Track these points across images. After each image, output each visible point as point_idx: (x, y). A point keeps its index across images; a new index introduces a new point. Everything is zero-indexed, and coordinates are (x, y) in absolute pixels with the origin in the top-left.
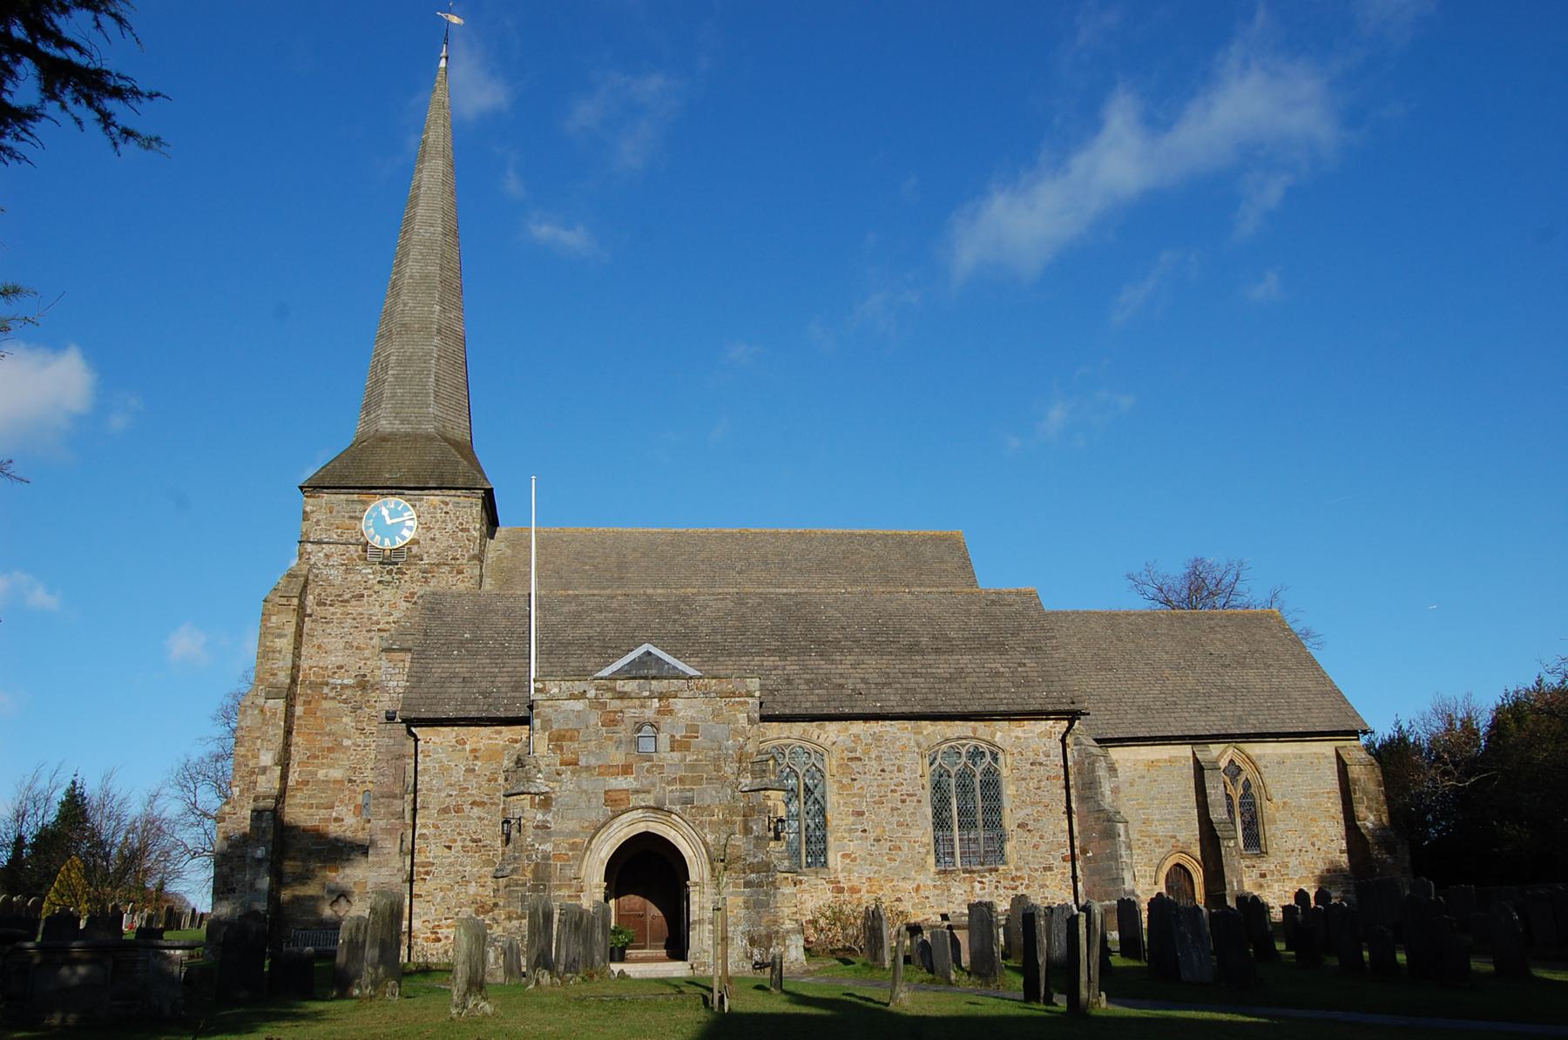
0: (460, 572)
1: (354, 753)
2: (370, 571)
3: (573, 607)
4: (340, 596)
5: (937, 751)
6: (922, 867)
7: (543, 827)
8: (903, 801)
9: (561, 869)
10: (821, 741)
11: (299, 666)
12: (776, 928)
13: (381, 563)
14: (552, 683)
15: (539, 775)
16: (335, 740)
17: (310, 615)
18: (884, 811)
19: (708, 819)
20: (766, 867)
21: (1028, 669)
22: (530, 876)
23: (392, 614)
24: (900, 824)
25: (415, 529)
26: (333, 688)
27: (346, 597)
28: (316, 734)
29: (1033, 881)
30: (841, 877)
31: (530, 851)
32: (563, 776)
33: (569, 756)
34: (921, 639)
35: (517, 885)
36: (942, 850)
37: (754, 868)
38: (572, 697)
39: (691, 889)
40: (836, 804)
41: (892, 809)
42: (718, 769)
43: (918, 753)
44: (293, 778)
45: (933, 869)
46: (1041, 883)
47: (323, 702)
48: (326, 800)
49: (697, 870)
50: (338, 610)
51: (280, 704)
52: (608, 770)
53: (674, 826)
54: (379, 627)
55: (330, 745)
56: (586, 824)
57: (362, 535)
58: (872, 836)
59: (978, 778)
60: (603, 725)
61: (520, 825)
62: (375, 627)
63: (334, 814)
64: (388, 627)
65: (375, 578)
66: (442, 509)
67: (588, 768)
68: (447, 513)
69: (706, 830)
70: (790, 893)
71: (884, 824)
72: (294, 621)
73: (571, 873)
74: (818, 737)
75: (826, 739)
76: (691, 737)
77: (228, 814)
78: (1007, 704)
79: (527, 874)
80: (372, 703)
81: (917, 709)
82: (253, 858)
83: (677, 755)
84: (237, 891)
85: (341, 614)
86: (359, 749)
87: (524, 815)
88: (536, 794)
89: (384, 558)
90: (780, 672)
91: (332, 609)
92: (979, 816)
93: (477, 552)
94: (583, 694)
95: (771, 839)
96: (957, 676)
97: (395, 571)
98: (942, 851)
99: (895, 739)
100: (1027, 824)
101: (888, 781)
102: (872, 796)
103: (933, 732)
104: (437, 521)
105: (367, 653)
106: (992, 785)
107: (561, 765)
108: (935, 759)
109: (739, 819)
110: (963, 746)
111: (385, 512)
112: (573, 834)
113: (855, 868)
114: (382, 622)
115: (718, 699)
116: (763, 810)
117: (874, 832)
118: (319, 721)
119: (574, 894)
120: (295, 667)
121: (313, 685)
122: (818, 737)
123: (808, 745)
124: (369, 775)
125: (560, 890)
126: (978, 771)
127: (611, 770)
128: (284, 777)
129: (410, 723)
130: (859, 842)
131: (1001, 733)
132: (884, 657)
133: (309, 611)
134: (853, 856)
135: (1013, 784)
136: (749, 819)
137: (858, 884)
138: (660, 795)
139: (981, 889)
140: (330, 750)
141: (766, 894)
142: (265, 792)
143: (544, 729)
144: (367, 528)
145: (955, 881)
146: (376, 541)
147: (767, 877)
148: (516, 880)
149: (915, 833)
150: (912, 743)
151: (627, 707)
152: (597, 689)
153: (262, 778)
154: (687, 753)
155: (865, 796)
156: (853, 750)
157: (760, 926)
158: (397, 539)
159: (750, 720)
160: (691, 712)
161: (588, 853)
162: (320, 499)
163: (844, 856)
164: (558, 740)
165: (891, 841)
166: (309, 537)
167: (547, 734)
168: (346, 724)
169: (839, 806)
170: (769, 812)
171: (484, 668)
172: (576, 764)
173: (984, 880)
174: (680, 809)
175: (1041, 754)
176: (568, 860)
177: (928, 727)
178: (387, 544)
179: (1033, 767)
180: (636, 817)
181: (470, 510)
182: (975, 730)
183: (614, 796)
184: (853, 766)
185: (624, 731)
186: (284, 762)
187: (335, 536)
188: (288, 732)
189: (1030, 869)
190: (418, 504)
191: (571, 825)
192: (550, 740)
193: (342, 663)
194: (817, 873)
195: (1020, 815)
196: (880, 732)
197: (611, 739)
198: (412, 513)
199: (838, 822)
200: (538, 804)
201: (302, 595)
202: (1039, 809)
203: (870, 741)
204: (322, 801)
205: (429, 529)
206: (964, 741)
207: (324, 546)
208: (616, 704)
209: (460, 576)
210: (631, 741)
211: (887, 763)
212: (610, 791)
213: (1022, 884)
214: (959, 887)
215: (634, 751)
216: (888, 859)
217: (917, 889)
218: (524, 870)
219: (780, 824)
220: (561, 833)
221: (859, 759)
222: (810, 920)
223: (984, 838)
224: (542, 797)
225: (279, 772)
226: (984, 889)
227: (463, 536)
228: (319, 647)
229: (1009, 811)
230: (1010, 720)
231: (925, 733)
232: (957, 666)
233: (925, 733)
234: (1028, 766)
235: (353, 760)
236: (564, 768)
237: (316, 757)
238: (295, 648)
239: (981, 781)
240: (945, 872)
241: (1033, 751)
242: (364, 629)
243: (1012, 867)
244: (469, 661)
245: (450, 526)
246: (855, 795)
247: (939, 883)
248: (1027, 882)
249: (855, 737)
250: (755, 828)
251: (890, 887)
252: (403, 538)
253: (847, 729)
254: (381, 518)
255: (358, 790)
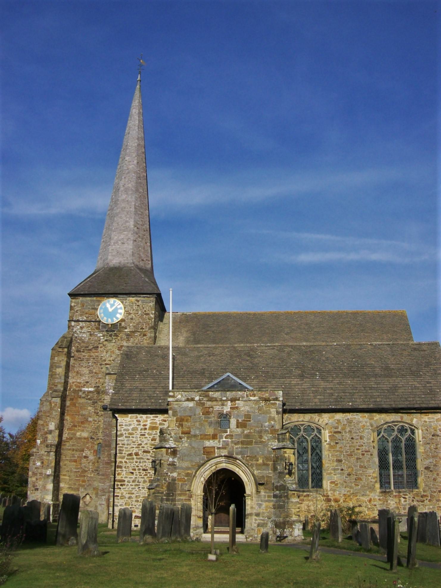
0: (145, 335)
1: (94, 425)
2: (101, 335)
3: (196, 353)
4: (87, 347)
5: (381, 429)
6: (372, 489)
7: (173, 464)
8: (363, 455)
9: (181, 486)
10: (320, 423)
11: (68, 382)
12: (288, 519)
13: (107, 331)
14: (178, 393)
15: (171, 439)
16: (85, 418)
17: (73, 357)
18: (353, 459)
19: (255, 462)
20: (283, 488)
21: (432, 385)
22: (165, 488)
23: (112, 356)
24: (361, 467)
25: (123, 314)
26: (84, 393)
27: (90, 347)
28: (76, 415)
29: (433, 498)
30: (329, 493)
31: (165, 476)
32: (183, 439)
33: (186, 429)
34: (375, 369)
35: (159, 493)
36: (384, 482)
37: (277, 488)
38: (188, 400)
39: (246, 498)
40: (327, 456)
41: (357, 459)
42: (261, 437)
43: (371, 429)
44: (65, 436)
45: (379, 491)
46: (437, 499)
47: (79, 399)
48: (80, 447)
49: (250, 488)
50: (86, 354)
51: (58, 400)
52: (206, 437)
53: (238, 466)
54: (105, 362)
55: (83, 420)
56: (194, 464)
57: (98, 317)
58: (346, 472)
59: (403, 442)
60: (203, 414)
61: (161, 464)
62: (104, 363)
63: (84, 454)
64: (109, 362)
65: (103, 339)
66: (136, 304)
67: (195, 436)
68: (138, 306)
69: (254, 468)
70: (296, 502)
71: (353, 467)
72: (65, 359)
73: (186, 488)
74: (318, 421)
75: (322, 422)
76: (247, 421)
77: (35, 452)
78: (419, 404)
79: (164, 488)
80: (102, 400)
81: (371, 406)
82: (45, 474)
83: (239, 430)
84: (39, 490)
85: (88, 356)
86: (96, 423)
87: (163, 458)
88: (169, 448)
89: (108, 329)
90: (300, 387)
91: (83, 354)
92: (404, 463)
93: (153, 324)
94: (192, 400)
95: (287, 474)
96: (394, 389)
97: (113, 334)
98: (384, 481)
99: (359, 422)
100: (430, 468)
101: (355, 444)
102: (346, 452)
103: (380, 418)
104: (134, 310)
105: (100, 376)
106: (411, 446)
107: (182, 433)
108: (380, 433)
109: (271, 463)
110: (395, 425)
111: (108, 306)
112: (188, 468)
113: (337, 489)
114: (107, 360)
115: (261, 402)
116: (283, 458)
117: (347, 470)
118: (77, 409)
119: (187, 498)
120: (66, 383)
121: (75, 391)
122: (318, 421)
123: (313, 425)
124: (100, 435)
125: (181, 496)
126: (403, 439)
127: (207, 437)
128: (60, 435)
129: (116, 411)
130: (339, 475)
131: (416, 419)
132: (355, 379)
133: (72, 355)
134: (336, 482)
135: (423, 446)
136: (276, 463)
137: (339, 497)
138: (231, 450)
139: (404, 501)
140: (82, 423)
141: (284, 502)
142: (52, 443)
143: (174, 415)
144: (100, 314)
145: (391, 497)
146: (104, 320)
147: (284, 493)
148: (158, 490)
149: (370, 471)
150: (368, 424)
151: (215, 405)
152: (200, 396)
153: (49, 436)
154: (245, 429)
155: (343, 452)
156: (337, 428)
157: (281, 517)
158: (114, 319)
159: (278, 413)
160: (247, 408)
161: (195, 478)
162: (78, 300)
163: (331, 483)
164: (181, 421)
165: (356, 475)
166: (73, 319)
167: (175, 418)
168: (90, 410)
169: (329, 457)
170: (286, 460)
171: (151, 384)
172: (189, 434)
173: (406, 497)
174: (241, 457)
175: (438, 430)
176: (185, 481)
177: (377, 416)
178: (110, 321)
179: (434, 437)
180: (219, 460)
181: (150, 304)
182: (402, 418)
183: (208, 450)
184: (337, 436)
185: (213, 418)
186: (61, 428)
187: (85, 318)
188: (62, 414)
189: (431, 491)
190: (124, 301)
191: (185, 464)
192: (177, 421)
193: (88, 381)
194: (317, 491)
195: (427, 462)
196: (351, 418)
197: (207, 421)
198: (122, 306)
199: (328, 465)
200: (170, 453)
201: (69, 347)
202: (437, 459)
203: (346, 423)
204: (78, 448)
205: (130, 314)
206: (396, 423)
207: (80, 323)
208: (209, 404)
209: (145, 337)
210: (217, 423)
211: (355, 435)
212: (206, 447)
213: (427, 499)
214: (392, 500)
215: (218, 427)
216: (355, 485)
217: (370, 501)
218: (162, 486)
219: (290, 466)
220: (182, 468)
221: (340, 432)
222: (313, 515)
223: (406, 475)
224: (172, 450)
225: (57, 433)
226: (406, 501)
227: (146, 317)
228: (77, 372)
229: (420, 460)
230: (421, 413)
231: (375, 419)
232: (394, 384)
233: (375, 419)
234: (431, 437)
235: (93, 428)
236: (183, 435)
237: (75, 426)
238: (65, 373)
239: (405, 445)
240: (385, 492)
241: (434, 429)
242: (99, 364)
243: (421, 490)
244: (143, 381)
245: (140, 312)
246: (337, 451)
247: (382, 498)
248: (429, 498)
249: (337, 421)
250: (279, 467)
251: (356, 499)
252: (117, 318)
253: (333, 417)
254: (106, 309)
255: (95, 443)
